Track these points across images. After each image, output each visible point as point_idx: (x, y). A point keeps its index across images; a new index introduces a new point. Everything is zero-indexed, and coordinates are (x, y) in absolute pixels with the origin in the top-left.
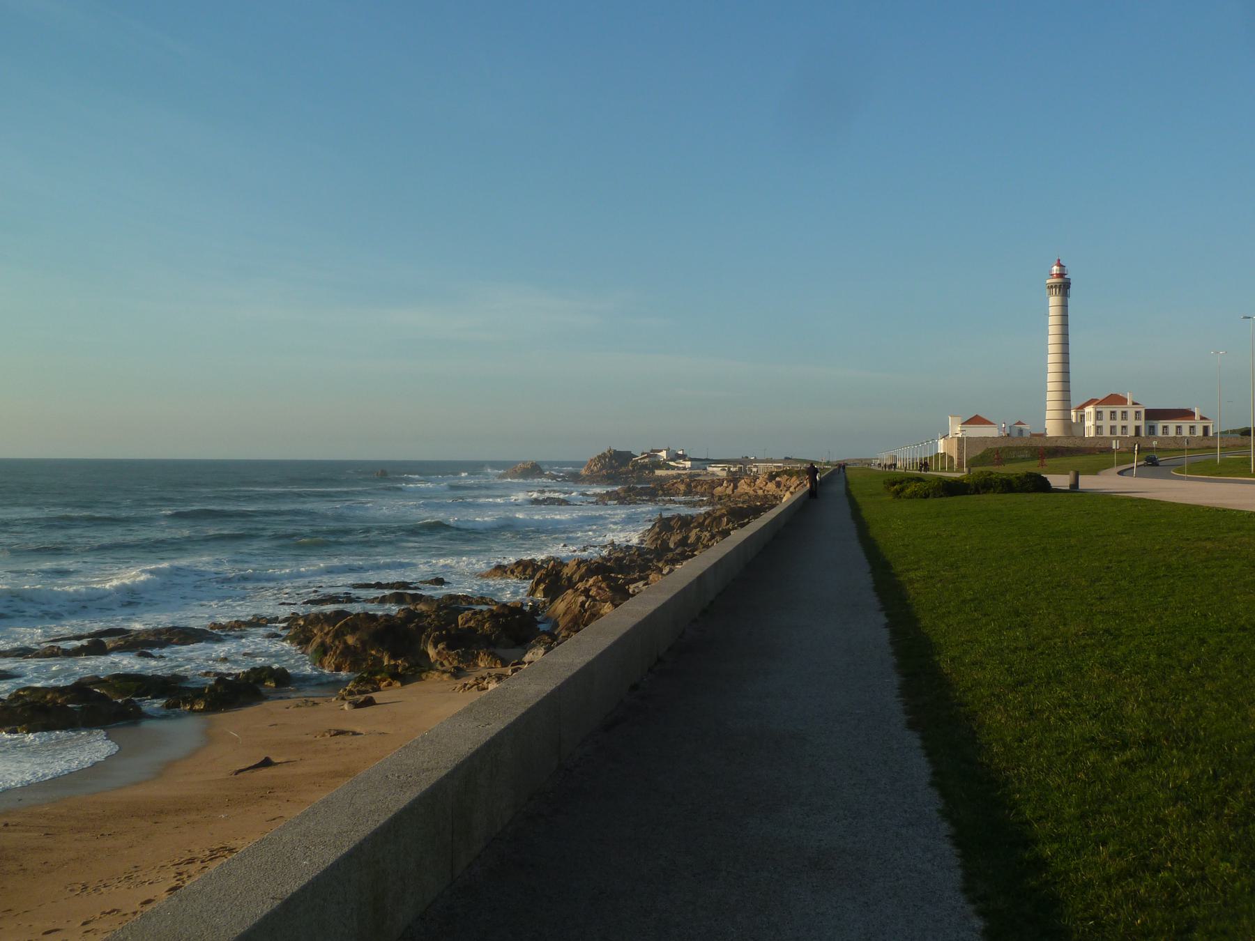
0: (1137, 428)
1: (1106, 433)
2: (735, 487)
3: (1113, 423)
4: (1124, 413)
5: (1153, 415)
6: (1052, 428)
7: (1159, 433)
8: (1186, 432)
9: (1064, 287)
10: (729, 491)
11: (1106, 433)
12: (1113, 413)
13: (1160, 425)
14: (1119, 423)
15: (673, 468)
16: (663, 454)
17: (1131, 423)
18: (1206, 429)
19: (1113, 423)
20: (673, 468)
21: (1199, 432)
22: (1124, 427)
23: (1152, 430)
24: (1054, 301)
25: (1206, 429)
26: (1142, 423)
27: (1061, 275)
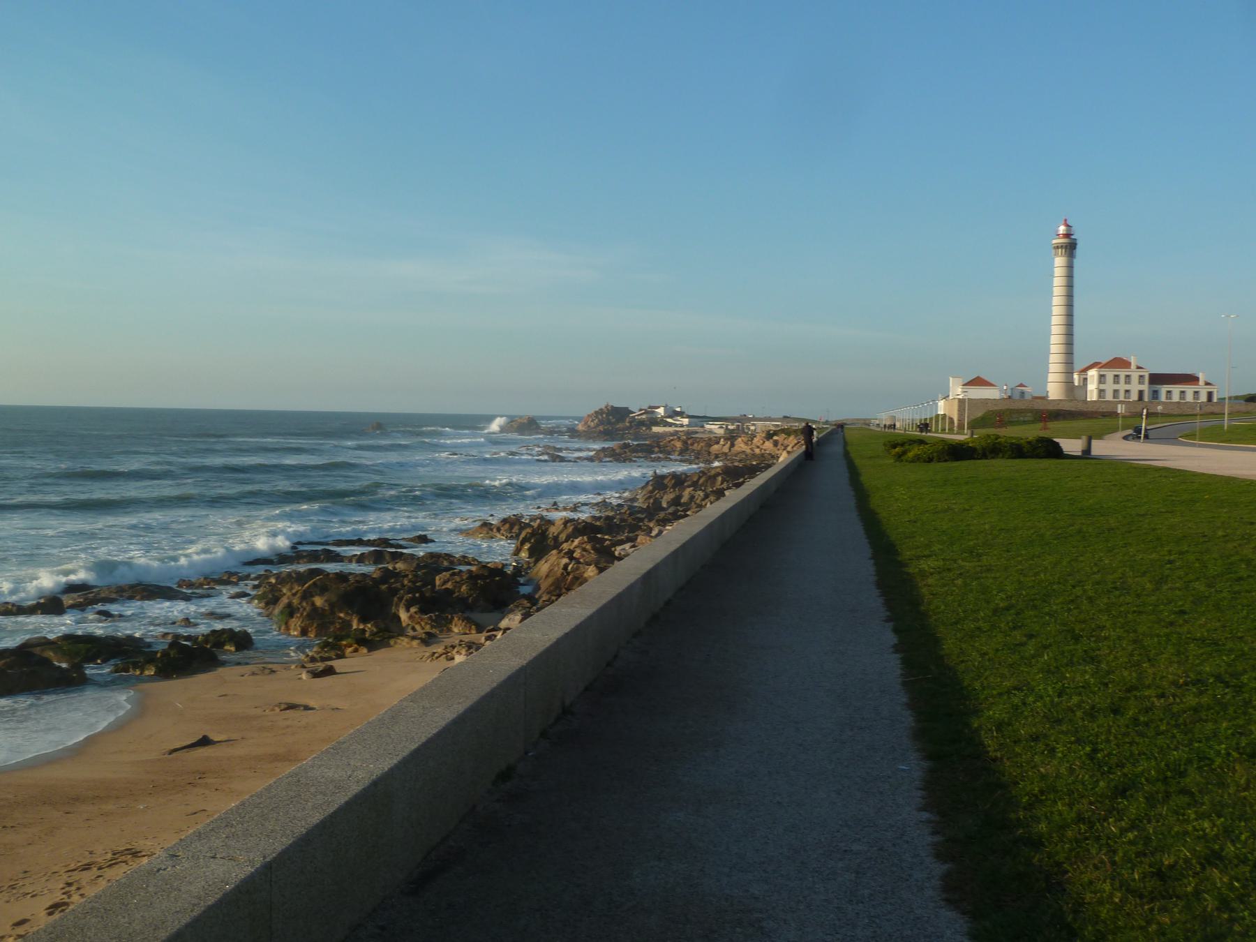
0: (1141, 393)
1: (1109, 397)
2: (732, 445)
3: (1116, 387)
4: (1128, 376)
5: (1157, 379)
6: (1054, 391)
7: (1163, 397)
8: (1189, 398)
9: (1070, 248)
10: (726, 449)
11: (1109, 397)
12: (1117, 376)
13: (1163, 389)
14: (1122, 387)
15: (671, 425)
16: (661, 411)
17: (1135, 387)
18: (1210, 395)
19: (1116, 387)
20: (671, 425)
21: (1203, 398)
22: (1127, 391)
23: (1155, 394)
24: (1060, 261)
25: (1210, 395)
26: (1145, 387)
27: (1067, 235)
